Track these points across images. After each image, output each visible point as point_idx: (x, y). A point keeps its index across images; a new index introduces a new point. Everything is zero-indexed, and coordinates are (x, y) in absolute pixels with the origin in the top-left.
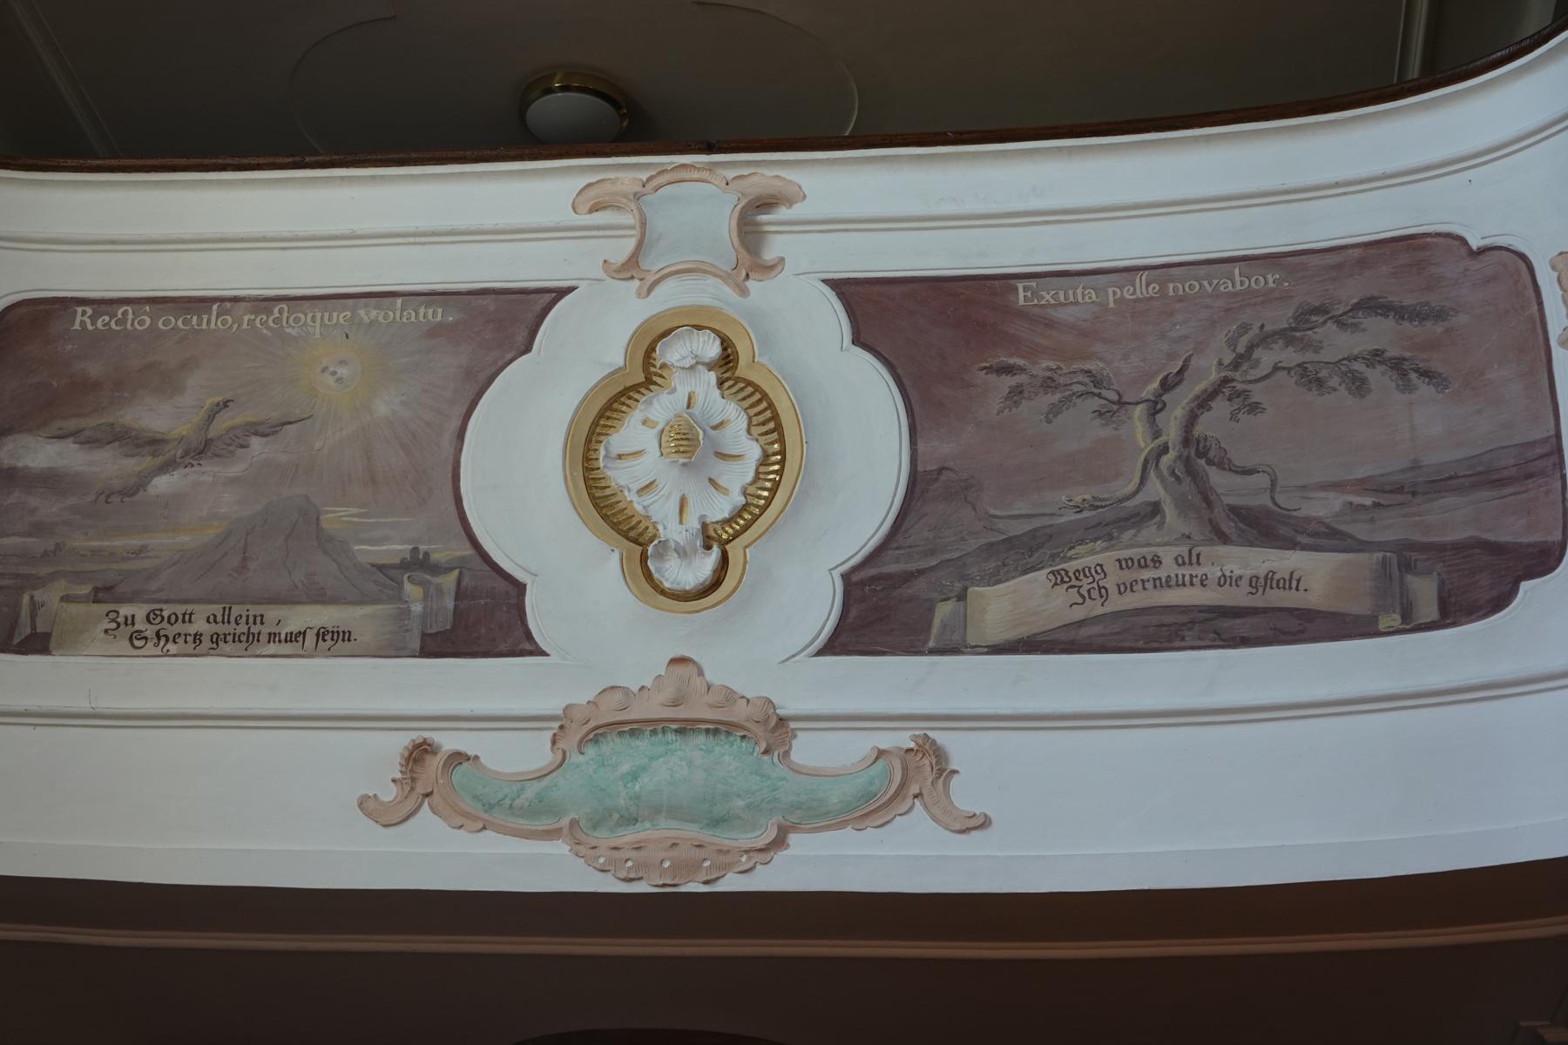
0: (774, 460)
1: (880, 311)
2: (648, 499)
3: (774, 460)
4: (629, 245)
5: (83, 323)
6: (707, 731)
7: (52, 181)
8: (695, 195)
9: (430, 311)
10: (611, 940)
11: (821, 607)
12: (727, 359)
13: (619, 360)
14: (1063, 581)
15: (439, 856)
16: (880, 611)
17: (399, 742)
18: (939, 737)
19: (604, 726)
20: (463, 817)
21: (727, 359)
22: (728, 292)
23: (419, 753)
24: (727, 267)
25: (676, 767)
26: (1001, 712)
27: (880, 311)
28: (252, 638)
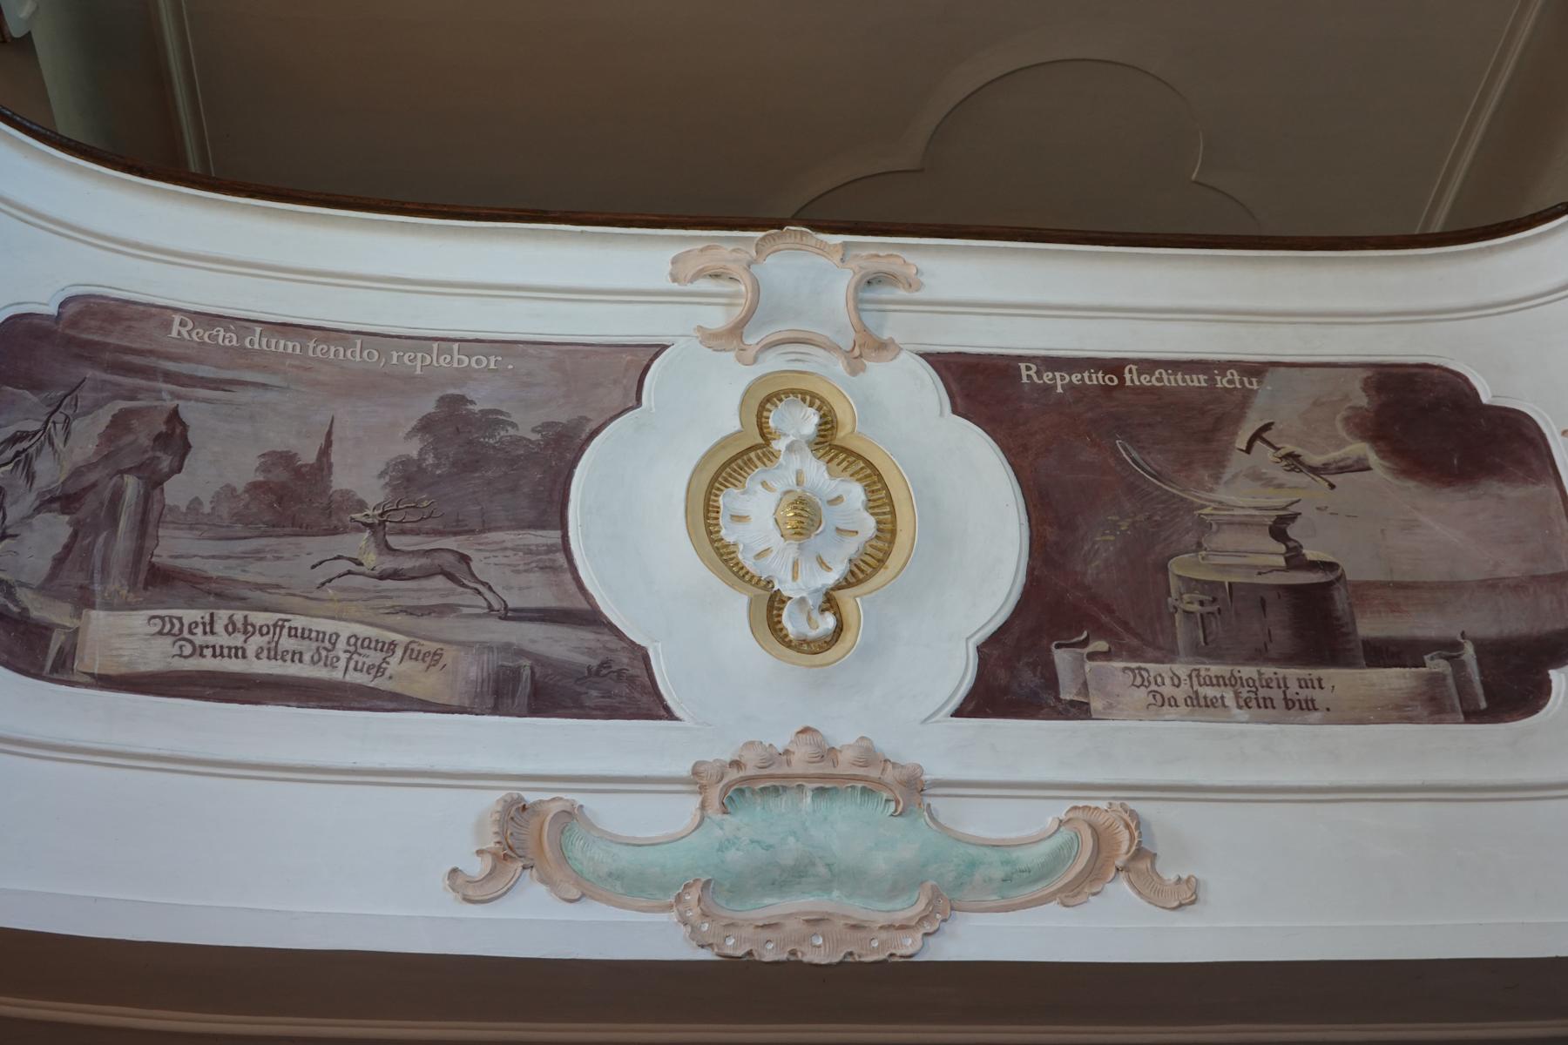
0: (880, 499)
1: (978, 385)
2: (764, 562)
3: (880, 499)
4: (738, 312)
5: (1029, 377)
6: (763, 790)
7: (1525, 239)
8: (812, 271)
9: (1086, 375)
10: (1257, 1027)
11: (957, 672)
12: (828, 424)
13: (733, 425)
14: (169, 633)
15: (534, 924)
16: (1010, 680)
17: (489, 800)
18: (1142, 808)
19: (743, 784)
20: (585, 888)
21: (828, 424)
22: (839, 367)
23: (517, 813)
24: (846, 344)
25: (845, 829)
26: (389, 766)
27: (978, 385)
28: (1309, 706)
